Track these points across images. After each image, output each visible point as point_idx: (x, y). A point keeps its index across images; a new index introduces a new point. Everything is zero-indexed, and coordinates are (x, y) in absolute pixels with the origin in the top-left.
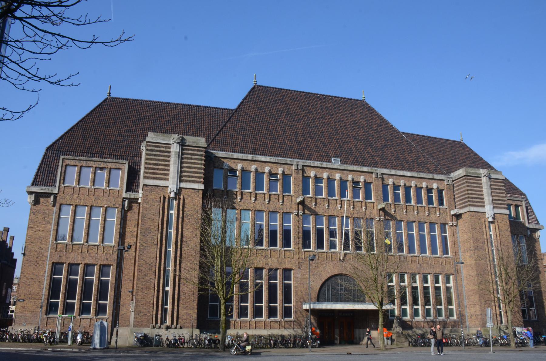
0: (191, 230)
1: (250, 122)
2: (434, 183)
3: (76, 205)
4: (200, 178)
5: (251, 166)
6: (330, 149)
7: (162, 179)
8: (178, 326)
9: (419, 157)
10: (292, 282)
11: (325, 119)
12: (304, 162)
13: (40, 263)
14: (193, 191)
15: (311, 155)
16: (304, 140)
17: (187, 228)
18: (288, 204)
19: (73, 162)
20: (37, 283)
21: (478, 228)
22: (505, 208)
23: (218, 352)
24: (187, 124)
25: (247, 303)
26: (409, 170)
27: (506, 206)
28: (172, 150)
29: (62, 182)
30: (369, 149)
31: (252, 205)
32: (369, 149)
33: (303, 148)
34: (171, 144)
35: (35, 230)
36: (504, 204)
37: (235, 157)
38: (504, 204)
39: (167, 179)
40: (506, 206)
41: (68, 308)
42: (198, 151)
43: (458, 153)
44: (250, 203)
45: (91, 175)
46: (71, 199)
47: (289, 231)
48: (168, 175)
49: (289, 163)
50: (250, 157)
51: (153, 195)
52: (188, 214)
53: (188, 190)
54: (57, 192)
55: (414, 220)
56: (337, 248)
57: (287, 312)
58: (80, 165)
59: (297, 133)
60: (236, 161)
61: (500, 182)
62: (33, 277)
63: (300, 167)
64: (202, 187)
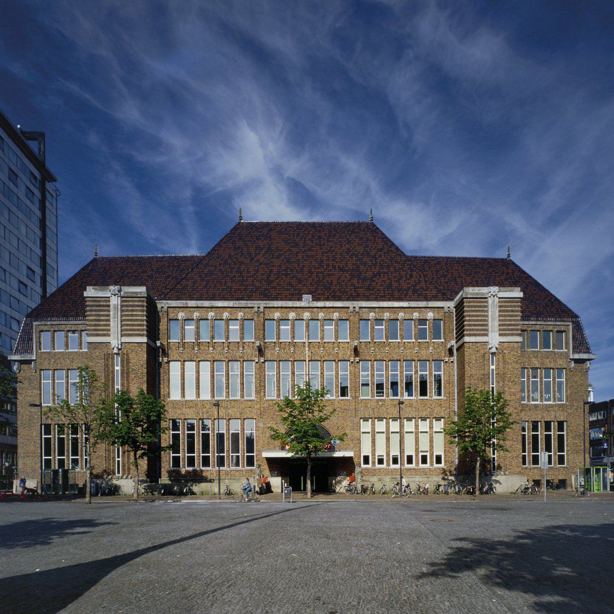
0: (136, 385)
1: (220, 264)
2: (415, 312)
3: (55, 370)
4: (142, 330)
5: (208, 313)
6: (304, 285)
7: (104, 335)
8: (130, 476)
9: (419, 283)
10: (565, 433)
11: (312, 251)
12: (266, 304)
13: (32, 425)
14: (136, 345)
15: (279, 294)
16: (277, 279)
17: (133, 383)
18: (249, 351)
19: (46, 328)
20: (33, 443)
21: (474, 362)
22: (517, 335)
23: (196, 499)
24: (169, 276)
25: (564, 452)
26: (399, 299)
27: (520, 332)
28: (111, 303)
29: (38, 348)
30: (355, 281)
31: (210, 356)
32: (355, 281)
33: (273, 287)
34: (109, 297)
35: (24, 396)
36: (517, 330)
37: (190, 306)
38: (517, 330)
39: (109, 335)
40: (520, 332)
41: (221, 461)
42: (139, 301)
43: (496, 273)
44: (208, 354)
45: (63, 339)
46: (49, 364)
47: (426, 382)
48: (109, 330)
49: (249, 306)
50: (206, 303)
51: (97, 353)
52: (133, 369)
53: (131, 344)
54: (35, 359)
55: (399, 358)
56: (443, 395)
57: (250, 461)
58: (52, 329)
59: (271, 271)
60: (192, 309)
61: (515, 302)
62: (29, 437)
63: (262, 309)
64: (145, 340)
